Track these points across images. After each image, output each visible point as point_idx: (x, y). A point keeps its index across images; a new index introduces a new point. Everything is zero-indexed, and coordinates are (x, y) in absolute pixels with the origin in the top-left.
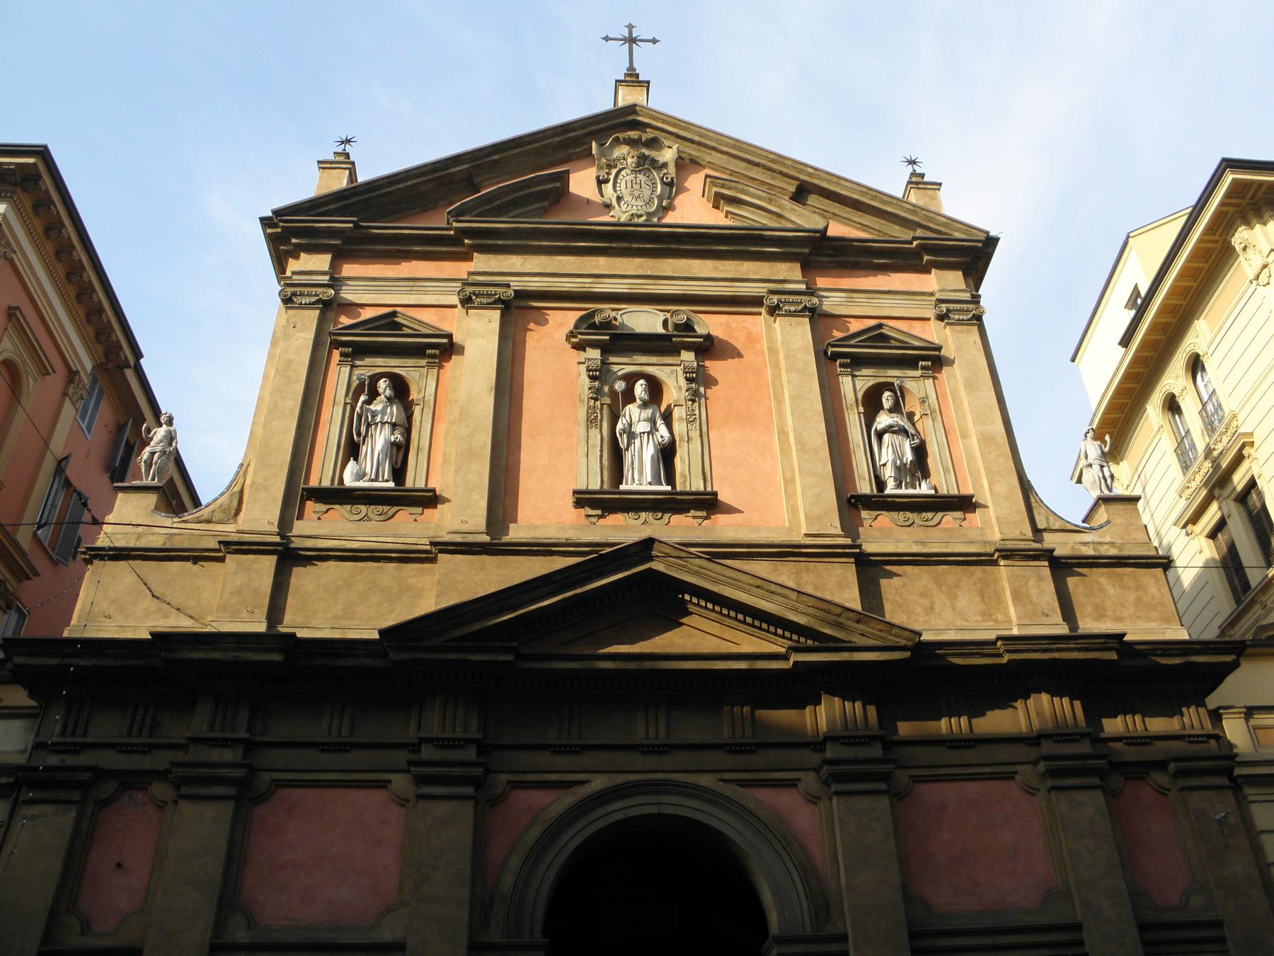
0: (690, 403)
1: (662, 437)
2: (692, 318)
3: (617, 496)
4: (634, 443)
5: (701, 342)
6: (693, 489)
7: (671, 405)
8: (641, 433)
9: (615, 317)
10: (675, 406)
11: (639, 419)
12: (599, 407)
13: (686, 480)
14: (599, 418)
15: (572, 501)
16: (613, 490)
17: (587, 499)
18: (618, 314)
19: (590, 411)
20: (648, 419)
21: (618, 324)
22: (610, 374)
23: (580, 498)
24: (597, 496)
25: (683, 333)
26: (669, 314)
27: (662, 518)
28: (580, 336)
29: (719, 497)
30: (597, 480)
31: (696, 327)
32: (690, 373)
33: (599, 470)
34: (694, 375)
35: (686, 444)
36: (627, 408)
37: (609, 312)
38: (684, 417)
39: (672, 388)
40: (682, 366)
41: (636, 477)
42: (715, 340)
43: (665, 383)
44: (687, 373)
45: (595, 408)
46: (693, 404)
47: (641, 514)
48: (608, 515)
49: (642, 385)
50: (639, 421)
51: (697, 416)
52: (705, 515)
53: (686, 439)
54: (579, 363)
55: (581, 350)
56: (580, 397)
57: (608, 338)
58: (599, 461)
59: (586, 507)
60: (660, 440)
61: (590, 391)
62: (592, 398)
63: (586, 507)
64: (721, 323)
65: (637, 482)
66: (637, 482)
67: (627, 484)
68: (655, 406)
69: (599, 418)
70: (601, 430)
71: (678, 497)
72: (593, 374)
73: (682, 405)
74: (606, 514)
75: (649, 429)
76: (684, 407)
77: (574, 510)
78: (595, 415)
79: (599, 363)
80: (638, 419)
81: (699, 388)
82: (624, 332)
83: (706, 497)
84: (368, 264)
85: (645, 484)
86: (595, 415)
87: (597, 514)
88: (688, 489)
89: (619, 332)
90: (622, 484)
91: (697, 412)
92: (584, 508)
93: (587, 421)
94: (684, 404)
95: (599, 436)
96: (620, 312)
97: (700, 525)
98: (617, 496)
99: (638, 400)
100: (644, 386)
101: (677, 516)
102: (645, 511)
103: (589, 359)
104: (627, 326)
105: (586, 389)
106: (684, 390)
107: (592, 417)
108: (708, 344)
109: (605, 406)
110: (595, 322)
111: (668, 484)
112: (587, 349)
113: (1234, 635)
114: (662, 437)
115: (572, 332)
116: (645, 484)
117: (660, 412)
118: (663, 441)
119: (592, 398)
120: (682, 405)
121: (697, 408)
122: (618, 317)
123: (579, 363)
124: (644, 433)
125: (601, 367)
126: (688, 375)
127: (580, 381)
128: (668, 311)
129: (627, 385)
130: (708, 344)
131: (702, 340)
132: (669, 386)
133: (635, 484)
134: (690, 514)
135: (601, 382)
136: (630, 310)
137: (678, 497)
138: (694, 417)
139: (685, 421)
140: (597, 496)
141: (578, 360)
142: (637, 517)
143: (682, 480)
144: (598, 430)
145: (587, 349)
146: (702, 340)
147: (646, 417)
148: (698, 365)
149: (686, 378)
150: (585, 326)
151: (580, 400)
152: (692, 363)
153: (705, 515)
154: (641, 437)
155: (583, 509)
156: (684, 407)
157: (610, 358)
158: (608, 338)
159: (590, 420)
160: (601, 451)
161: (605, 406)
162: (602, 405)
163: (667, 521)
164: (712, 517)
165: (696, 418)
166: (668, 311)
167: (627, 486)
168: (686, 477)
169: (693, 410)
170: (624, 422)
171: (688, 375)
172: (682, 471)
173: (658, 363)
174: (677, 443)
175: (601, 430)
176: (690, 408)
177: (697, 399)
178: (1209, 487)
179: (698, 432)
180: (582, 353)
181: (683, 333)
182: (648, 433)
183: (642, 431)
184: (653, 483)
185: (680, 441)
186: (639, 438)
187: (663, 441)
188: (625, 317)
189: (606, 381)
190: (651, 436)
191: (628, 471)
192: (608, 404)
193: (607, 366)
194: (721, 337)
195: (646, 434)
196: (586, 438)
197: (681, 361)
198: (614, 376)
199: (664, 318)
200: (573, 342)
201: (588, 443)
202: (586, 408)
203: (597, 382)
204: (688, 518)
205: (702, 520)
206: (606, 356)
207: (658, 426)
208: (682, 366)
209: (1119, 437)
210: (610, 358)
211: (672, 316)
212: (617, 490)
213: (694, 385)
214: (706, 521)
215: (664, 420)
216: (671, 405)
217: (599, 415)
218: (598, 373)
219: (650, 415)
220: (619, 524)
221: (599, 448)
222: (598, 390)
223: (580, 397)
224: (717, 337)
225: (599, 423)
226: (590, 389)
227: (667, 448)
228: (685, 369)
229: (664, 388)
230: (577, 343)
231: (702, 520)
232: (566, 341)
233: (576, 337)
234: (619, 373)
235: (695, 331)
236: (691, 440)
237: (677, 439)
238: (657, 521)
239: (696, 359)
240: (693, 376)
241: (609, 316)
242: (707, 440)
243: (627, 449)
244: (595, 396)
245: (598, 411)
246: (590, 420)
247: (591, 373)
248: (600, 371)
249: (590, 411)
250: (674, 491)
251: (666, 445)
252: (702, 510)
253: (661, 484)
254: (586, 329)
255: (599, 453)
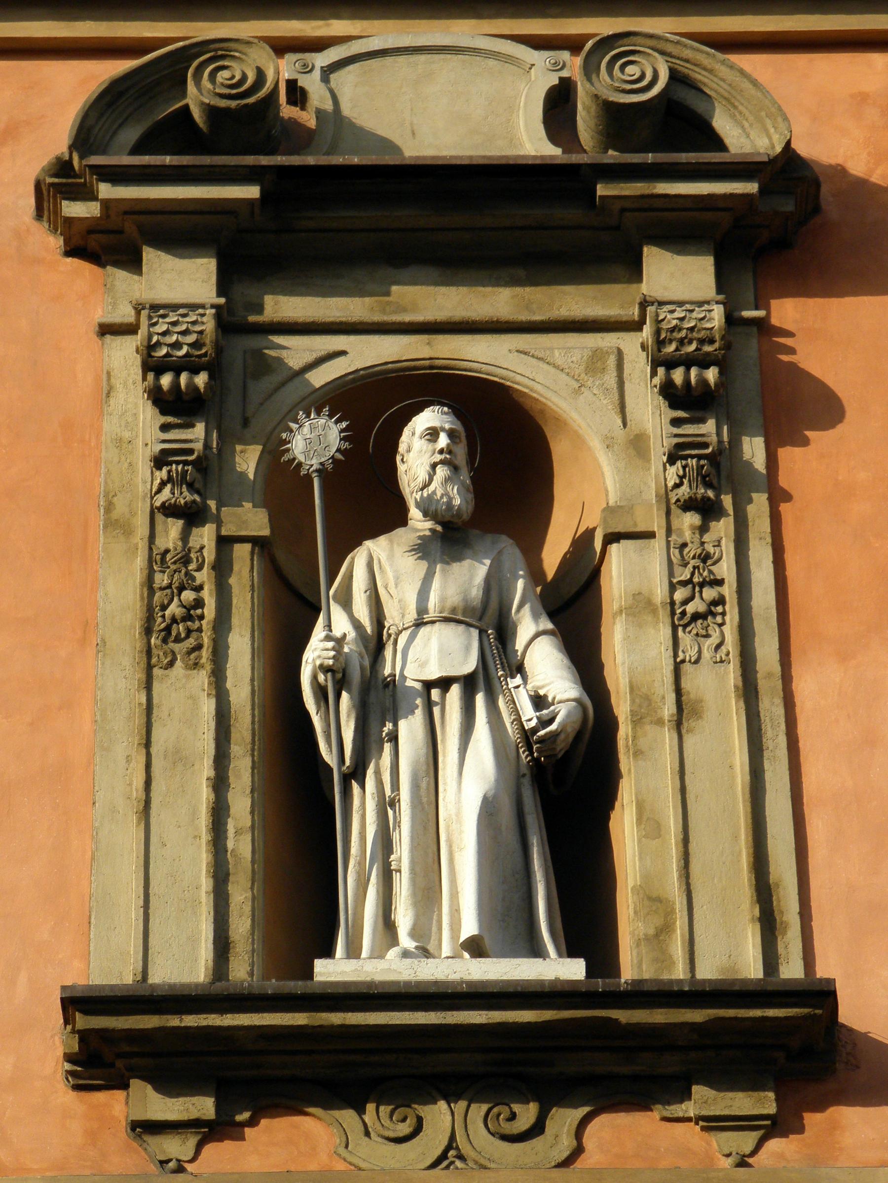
0: (691, 519)
1: (539, 701)
2: (699, 76)
3: (299, 1019)
4: (394, 738)
5: (745, 197)
6: (702, 974)
7: (590, 534)
8: (428, 685)
9: (292, 85)
10: (612, 538)
11: (422, 610)
12: (209, 555)
13: (665, 930)
14: (210, 611)
15: (60, 1052)
16: (273, 986)
17: (131, 1035)
18: (308, 70)
19: (161, 579)
20: (468, 610)
21: (312, 123)
22: (268, 382)
23: (104, 1034)
24: (191, 1021)
25: (650, 157)
26: (578, 61)
27: (537, 1129)
28: (105, 190)
29: (846, 1015)
30: (193, 941)
31: (722, 123)
32: (688, 362)
33: (206, 884)
34: (712, 375)
35: (668, 737)
36: (358, 560)
37: (262, 57)
38: (660, 593)
39: (596, 444)
40: (647, 331)
41: (404, 918)
42: (824, 189)
43: (560, 422)
44: (670, 364)
45: (185, 560)
46: (703, 529)
47: (425, 1111)
48: (252, 1122)
49: (433, 434)
50: (419, 624)
51: (729, 590)
52: (771, 1108)
53: (668, 709)
54: (107, 330)
55: (117, 264)
56: (109, 508)
57: (252, 192)
58: (205, 836)
59: (135, 1083)
60: (529, 714)
61: (163, 474)
62: (170, 510)
63: (135, 1083)
64: (862, 98)
65: (406, 941)
66: (406, 941)
67: (353, 952)
68: (506, 544)
69: (210, 611)
70: (218, 675)
71: (623, 1016)
72: (176, 384)
73: (651, 535)
74: (245, 1116)
75: (470, 665)
76: (658, 545)
77: (66, 1097)
78: (188, 596)
79: (209, 325)
80: (411, 615)
81: (735, 443)
82: (338, 160)
83: (771, 1013)
84: (225, 186)
85: (446, 950)
86: (188, 596)
87: (194, 1114)
88: (679, 972)
89: (311, 160)
90: (328, 952)
91: (726, 569)
92: (125, 1086)
93: (148, 631)
94: (657, 524)
95: (208, 707)
96: (322, 59)
97: (742, 1163)
98: (299, 1019)
99: (415, 513)
100: (443, 441)
101: (622, 1119)
102: (450, 1097)
103: (155, 307)
104: (352, 125)
105: (143, 467)
106: (658, 452)
107: (174, 609)
108: (788, 206)
109: (242, 551)
110: (186, 108)
111: (571, 951)
112: (149, 254)
113: (163, 484)
114: (539, 701)
115: (62, 167)
116: (446, 950)
117: (536, 573)
118: (546, 722)
119: (170, 510)
120: (651, 535)
121: (728, 549)
122: (312, 83)
123: (107, 330)
124: (445, 683)
125: (219, 349)
126: (678, 376)
127: (111, 426)
128: (573, 44)
129: (352, 436)
130: (788, 206)
131: (752, 187)
132: (579, 441)
133: (392, 953)
134: (689, 1109)
135: (217, 424)
136: (375, 44)
137: (623, 1016)
138: (709, 593)
139: (664, 615)
140: (191, 1021)
141: (101, 314)
142: (404, 1129)
143: (644, 928)
144: (202, 678)
145: (149, 254)
146: (752, 187)
147: (454, 598)
148: (731, 320)
149: (668, 391)
150: (131, 134)
151: (110, 524)
152: (698, 314)
153: (771, 1108)
154: (429, 705)
155: (120, 1095)
156: (658, 545)
157: (269, 301)
158: (252, 192)
159: (159, 624)
160: (220, 784)
161: (242, 551)
162: (224, 543)
163: (566, 1144)
164: (811, 1119)
165: (720, 601)
166: (573, 44)
167: (353, 964)
168: (669, 913)
169: (705, 558)
170: (341, 625)
171: (678, 376)
172: (646, 877)
173: (524, 317)
174: (624, 731)
175: (218, 675)
176: (692, 550)
177: (727, 501)
178: (298, 89)
179: (732, 674)
180: (120, 277)
181: (650, 157)
182: (469, 683)
183: (434, 673)
184: (488, 943)
185: (637, 720)
186: (419, 712)
187: (546, 722)
188: (343, 81)
189: (246, 422)
190: (480, 699)
191: (363, 887)
192: (255, 541)
193: (253, 342)
194: (857, 168)
195: (455, 691)
196: (139, 720)
197: (644, 304)
198: (291, 393)
199: (553, 80)
200: (69, 221)
201: (148, 745)
202: (140, 561)
203: (199, 430)
204: (680, 1127)
205: (755, 1135)
206: (243, 290)
207: (520, 645)
208: (647, 331)
209: (477, 51)
210: (269, 301)
211: (590, 69)
212: (297, 986)
213: (709, 427)
214: (774, 1145)
215: (552, 615)
216: (590, 534)
217: (209, 597)
218: (201, 380)
219: (476, 593)
220: (313, 1167)
221: (207, 770)
222: (202, 465)
223: (109, 508)
224: (840, 171)
225: (206, 640)
226: (159, 461)
227: (569, 754)
228: (660, 343)
229: (559, 449)
230: (92, 227)
231: (755, 1135)
232: (39, 213)
233: (86, 194)
234: (319, 378)
235: (717, 143)
236: (697, 713)
237: (622, 708)
238: (505, 1145)
239: (720, 288)
240: (703, 382)
241: (261, 75)
242: (779, 711)
243: (357, 773)
244: (186, 496)
245: (204, 576)
246: (159, 624)
247: (166, 380)
248: (214, 368)
249: (161, 579)
250: (600, 984)
251: (561, 746)
252: (753, 1085)
253: (536, 951)
254: (136, 150)
255: (205, 795)
